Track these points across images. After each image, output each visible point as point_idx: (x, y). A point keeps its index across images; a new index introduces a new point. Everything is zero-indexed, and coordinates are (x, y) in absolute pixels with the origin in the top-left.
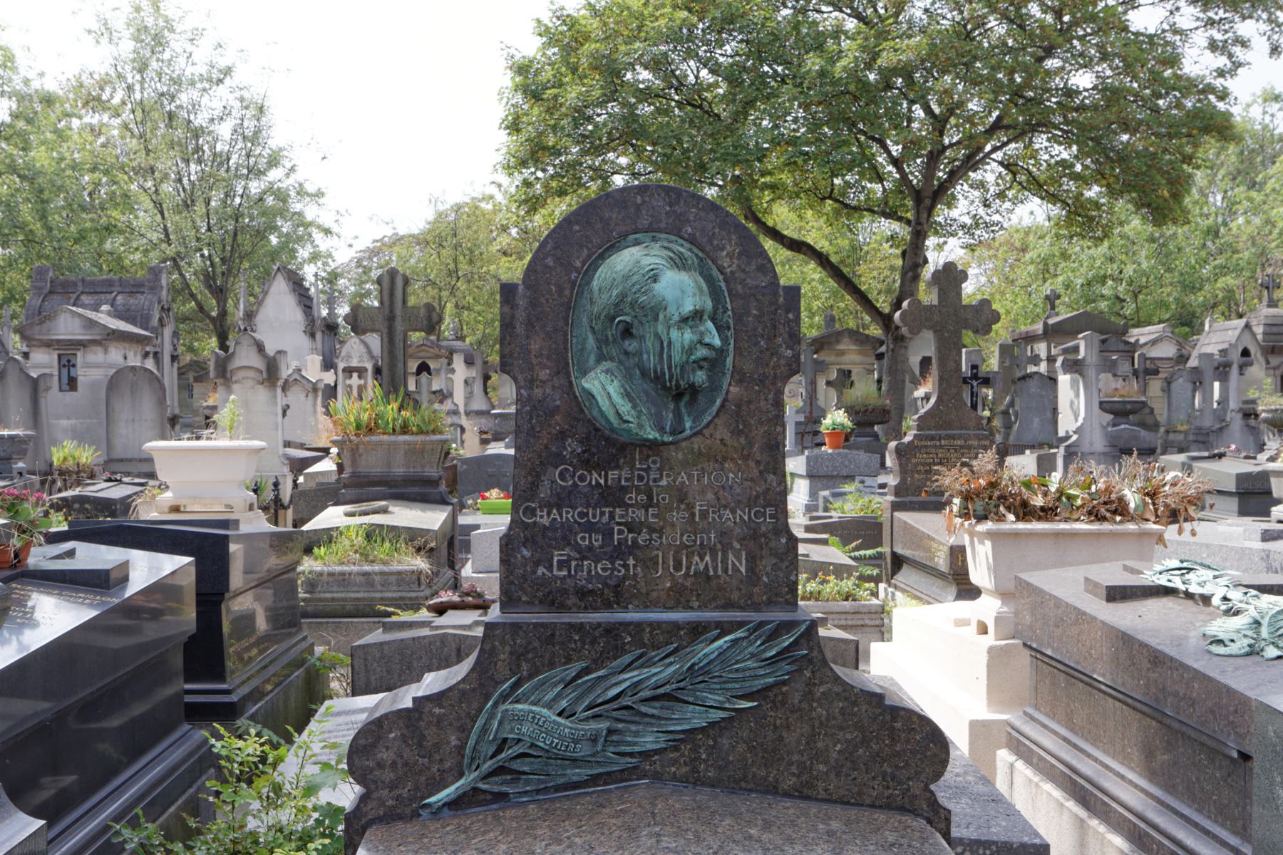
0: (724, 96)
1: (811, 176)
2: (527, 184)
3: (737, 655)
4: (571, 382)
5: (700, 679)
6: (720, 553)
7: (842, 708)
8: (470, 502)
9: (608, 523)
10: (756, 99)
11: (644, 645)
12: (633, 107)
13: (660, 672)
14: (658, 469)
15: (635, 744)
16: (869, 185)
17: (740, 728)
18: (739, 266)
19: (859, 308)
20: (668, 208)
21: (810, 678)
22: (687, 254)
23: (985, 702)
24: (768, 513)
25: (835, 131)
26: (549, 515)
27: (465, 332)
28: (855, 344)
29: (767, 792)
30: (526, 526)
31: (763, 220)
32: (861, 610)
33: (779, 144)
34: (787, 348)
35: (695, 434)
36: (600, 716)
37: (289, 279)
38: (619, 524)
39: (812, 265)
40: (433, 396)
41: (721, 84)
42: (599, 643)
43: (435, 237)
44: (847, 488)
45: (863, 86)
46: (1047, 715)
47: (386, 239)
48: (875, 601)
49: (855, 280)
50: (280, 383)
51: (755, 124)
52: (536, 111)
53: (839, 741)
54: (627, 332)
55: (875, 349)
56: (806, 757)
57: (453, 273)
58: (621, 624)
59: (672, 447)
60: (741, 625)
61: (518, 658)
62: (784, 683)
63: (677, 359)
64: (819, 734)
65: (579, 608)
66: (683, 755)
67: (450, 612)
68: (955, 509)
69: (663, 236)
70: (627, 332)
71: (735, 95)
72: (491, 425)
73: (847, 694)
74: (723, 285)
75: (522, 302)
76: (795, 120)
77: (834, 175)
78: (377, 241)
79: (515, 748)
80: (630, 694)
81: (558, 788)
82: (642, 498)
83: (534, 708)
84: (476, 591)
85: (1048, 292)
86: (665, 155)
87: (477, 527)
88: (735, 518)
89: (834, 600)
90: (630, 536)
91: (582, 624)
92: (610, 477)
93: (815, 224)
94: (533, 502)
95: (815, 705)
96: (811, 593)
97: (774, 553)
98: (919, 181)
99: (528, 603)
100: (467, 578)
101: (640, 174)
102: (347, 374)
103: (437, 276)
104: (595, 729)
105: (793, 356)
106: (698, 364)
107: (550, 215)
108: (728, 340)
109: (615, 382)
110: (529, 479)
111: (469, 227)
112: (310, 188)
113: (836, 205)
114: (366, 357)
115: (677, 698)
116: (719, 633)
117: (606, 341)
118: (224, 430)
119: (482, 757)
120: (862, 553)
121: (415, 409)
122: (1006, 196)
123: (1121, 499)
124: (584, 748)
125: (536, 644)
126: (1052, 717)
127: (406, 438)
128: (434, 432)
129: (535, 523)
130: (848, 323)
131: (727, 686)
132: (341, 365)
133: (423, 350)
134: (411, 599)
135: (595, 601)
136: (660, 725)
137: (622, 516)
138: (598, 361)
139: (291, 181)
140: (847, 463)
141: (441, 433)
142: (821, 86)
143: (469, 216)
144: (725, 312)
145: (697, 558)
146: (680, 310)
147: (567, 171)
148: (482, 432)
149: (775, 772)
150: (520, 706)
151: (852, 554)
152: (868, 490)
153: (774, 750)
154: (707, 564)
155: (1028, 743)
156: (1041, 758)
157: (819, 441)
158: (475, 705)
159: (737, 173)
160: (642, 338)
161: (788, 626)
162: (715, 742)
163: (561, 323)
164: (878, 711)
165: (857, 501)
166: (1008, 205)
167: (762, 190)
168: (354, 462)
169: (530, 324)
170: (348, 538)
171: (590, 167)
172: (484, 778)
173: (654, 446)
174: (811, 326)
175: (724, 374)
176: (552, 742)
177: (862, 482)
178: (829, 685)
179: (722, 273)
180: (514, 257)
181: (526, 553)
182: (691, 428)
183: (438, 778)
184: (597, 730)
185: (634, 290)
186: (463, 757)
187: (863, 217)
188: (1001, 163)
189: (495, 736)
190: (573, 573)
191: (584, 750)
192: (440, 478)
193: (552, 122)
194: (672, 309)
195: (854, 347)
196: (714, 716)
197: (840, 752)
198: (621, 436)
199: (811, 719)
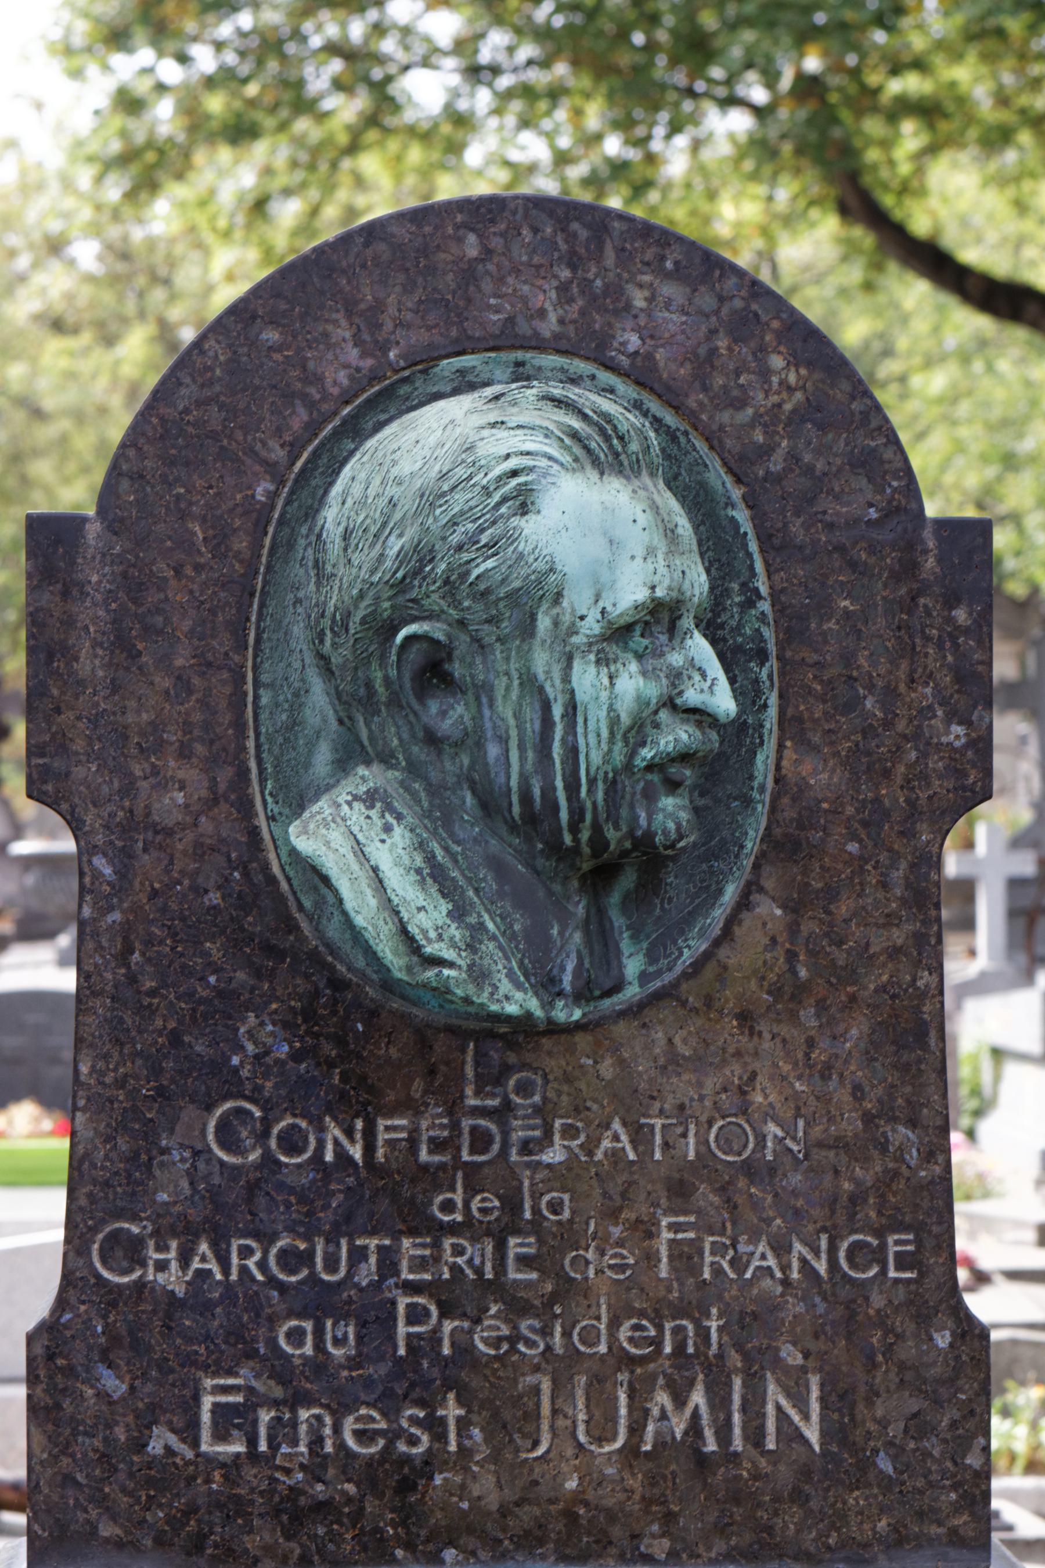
22: (628, 420)
31: (898, 215)
74: (742, 516)
107: (203, 203)
160: (483, 691)
163: (221, 643)
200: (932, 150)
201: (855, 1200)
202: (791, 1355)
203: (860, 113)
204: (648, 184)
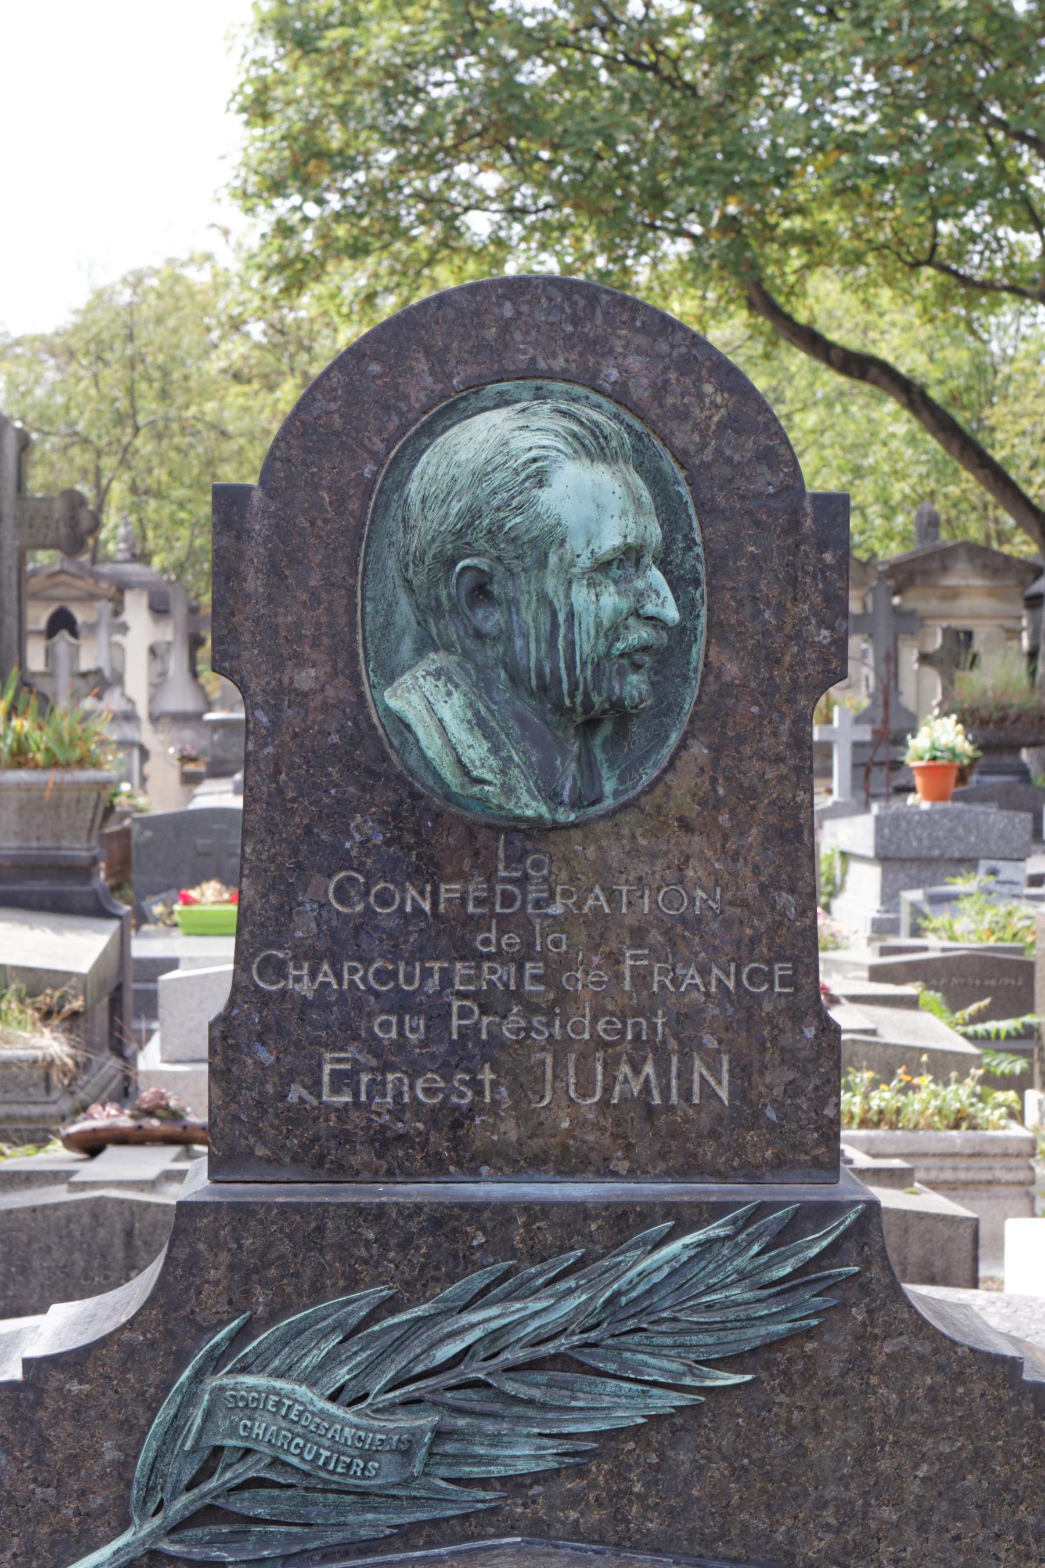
0: (704, 45)
1: (890, 215)
2: (284, 230)
3: (710, 1275)
4: (361, 696)
5: (631, 1324)
6: (675, 1059)
7: (931, 1388)
8: (158, 909)
9: (439, 994)
10: (774, 51)
11: (513, 1253)
12: (509, 67)
14: (545, 880)
15: (493, 1461)
16: (1013, 236)
17: (715, 1430)
18: (718, 451)
19: (990, 498)
20: (570, 329)
21: (864, 1325)
22: (610, 426)
24: (778, 973)
25: (943, 120)
26: (313, 976)
27: (151, 545)
28: (983, 576)
30: (265, 999)
31: (787, 309)
32: (987, 1148)
33: (821, 148)
34: (819, 626)
35: (625, 807)
36: (419, 1401)
38: (462, 995)
39: (891, 405)
40: (80, 683)
41: (699, 19)
42: (418, 1248)
43: (88, 342)
44: (960, 885)
45: (1003, 27)
48: (1015, 1130)
49: (982, 438)
51: (770, 105)
52: (304, 73)
53: (924, 1458)
55: (1023, 585)
56: (854, 1492)
57: (126, 418)
58: (464, 1206)
59: (576, 835)
60: (718, 1210)
61: (247, 1278)
62: (808, 1334)
63: (587, 648)
64: (883, 1442)
65: (377, 1172)
66: (592, 1485)
67: (112, 1152)
69: (559, 386)
71: (728, 43)
72: (204, 743)
73: (942, 1359)
74: (684, 490)
75: (258, 526)
76: (859, 95)
77: (936, 215)
79: (240, 1468)
80: (482, 1355)
83: (279, 1384)
84: (167, 1108)
86: (578, 170)
87: (172, 964)
88: (707, 985)
89: (930, 1126)
90: (486, 1020)
91: (381, 1206)
92: (443, 896)
93: (898, 317)
94: (280, 947)
95: (874, 1380)
96: (881, 1112)
97: (788, 1057)
99: (269, 1161)
100: (150, 1075)
101: (524, 211)
103: (92, 424)
104: (408, 1430)
105: (833, 642)
106: (632, 659)
107: (332, 297)
108: (694, 607)
109: (456, 695)
110: (273, 899)
111: (159, 321)
113: (942, 278)
115: (582, 1364)
116: (673, 1228)
117: (437, 610)
119: (169, 1487)
120: (992, 1026)
121: (41, 713)
124: (385, 1469)
125: (285, 1248)
127: (23, 776)
128: (81, 763)
129: (284, 992)
130: (965, 530)
131: (687, 1339)
133: (61, 584)
134: (29, 1119)
135: (409, 1158)
136: (546, 1422)
137: (467, 980)
138: (420, 651)
140: (960, 831)
141: (96, 765)
142: (911, 25)
143: (160, 296)
144: (689, 548)
145: (625, 1069)
146: (594, 546)
147: (370, 204)
148: (185, 759)
149: (789, 1522)
150: (249, 1380)
151: (970, 1029)
152: (1005, 889)
153: (786, 1476)
154: (647, 1080)
157: (901, 781)
158: (154, 1377)
159: (732, 209)
160: (512, 604)
162: (662, 1457)
163: (341, 571)
164: (1007, 1394)
165: (981, 912)
167: (784, 245)
169: (274, 571)
171: (418, 196)
172: (175, 1530)
174: (889, 536)
175: (686, 679)
176: (318, 1455)
177: (993, 872)
178: (904, 1339)
179: (683, 467)
180: (256, 385)
181: (266, 1057)
182: (616, 793)
183: (75, 1531)
184: (413, 1432)
185: (495, 503)
186: (129, 1485)
187: (999, 303)
189: (197, 1442)
190: (363, 1098)
192: (94, 861)
193: (338, 100)
194: (576, 544)
195: (978, 582)
196: (659, 1403)
197: (925, 1480)
198: (467, 808)
199: (864, 1411)
201: (754, 941)
202: (710, 1042)
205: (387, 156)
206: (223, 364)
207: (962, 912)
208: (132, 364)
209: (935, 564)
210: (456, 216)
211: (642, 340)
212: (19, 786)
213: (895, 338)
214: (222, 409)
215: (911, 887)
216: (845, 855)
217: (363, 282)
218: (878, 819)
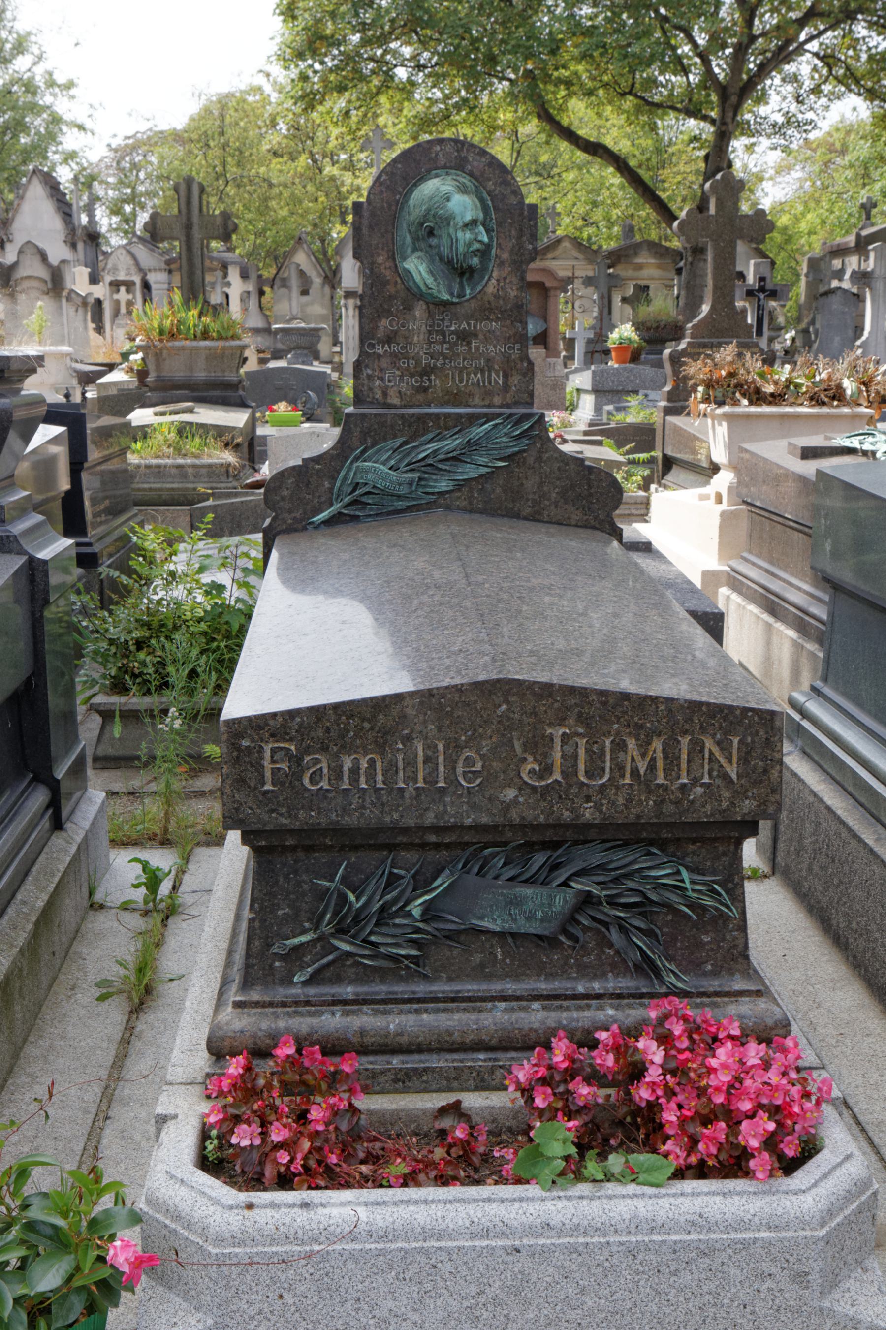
2: (304, 78)
11: (440, 428)
13: (451, 444)
22: (468, 183)
23: (716, 557)
28: (655, 258)
29: (512, 517)
31: (558, 118)
37: (46, 183)
46: (757, 556)
47: (139, 135)
50: (65, 294)
54: (431, 233)
62: (524, 451)
68: (699, 395)
70: (431, 233)
74: (490, 203)
75: (366, 214)
78: (129, 138)
81: (389, 513)
82: (440, 337)
85: (865, 200)
98: (726, 75)
102: (114, 288)
106: (475, 253)
107: (328, 113)
112: (60, 79)
113: (636, 101)
114: (133, 269)
118: (32, 335)
120: (637, 456)
121: (214, 316)
122: (821, 91)
123: (839, 387)
125: (376, 426)
126: (759, 556)
127: (207, 343)
130: (649, 235)
132: (108, 278)
139: (39, 70)
141: (239, 339)
152: (651, 404)
155: (740, 578)
156: (749, 587)
160: (440, 237)
161: (527, 417)
163: (390, 228)
165: (639, 413)
166: (823, 101)
168: (158, 367)
169: (371, 227)
170: (162, 433)
173: (446, 304)
174: (610, 238)
180: (285, 158)
187: (667, 114)
188: (816, 55)
191: (404, 490)
193: (331, 8)
194: (458, 219)
195: (653, 261)
200: (569, 96)
201: (509, 338)
202: (496, 367)
203: (545, 83)
204: (475, 107)
205: (356, 38)
206: (268, 147)
207: (630, 413)
208: (224, 147)
209: (632, 252)
210: (391, 70)
211: (478, 158)
212: (206, 348)
213: (615, 132)
214: (269, 171)
215: (606, 404)
216: (578, 390)
217: (343, 105)
218: (593, 372)
